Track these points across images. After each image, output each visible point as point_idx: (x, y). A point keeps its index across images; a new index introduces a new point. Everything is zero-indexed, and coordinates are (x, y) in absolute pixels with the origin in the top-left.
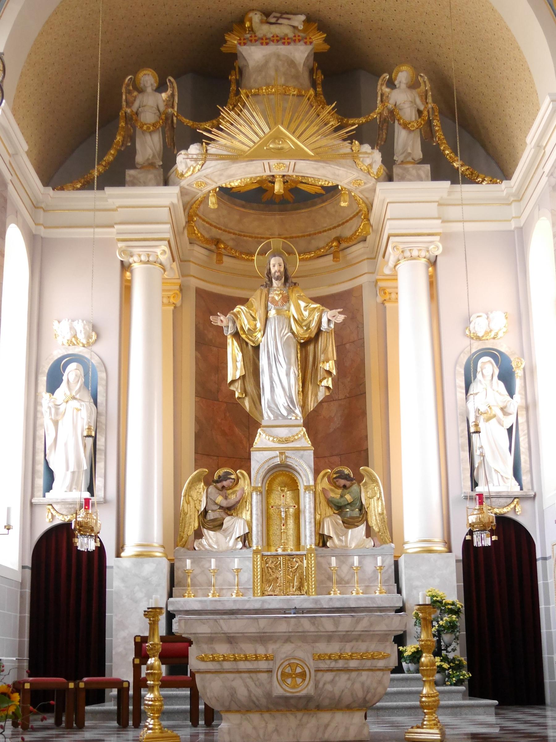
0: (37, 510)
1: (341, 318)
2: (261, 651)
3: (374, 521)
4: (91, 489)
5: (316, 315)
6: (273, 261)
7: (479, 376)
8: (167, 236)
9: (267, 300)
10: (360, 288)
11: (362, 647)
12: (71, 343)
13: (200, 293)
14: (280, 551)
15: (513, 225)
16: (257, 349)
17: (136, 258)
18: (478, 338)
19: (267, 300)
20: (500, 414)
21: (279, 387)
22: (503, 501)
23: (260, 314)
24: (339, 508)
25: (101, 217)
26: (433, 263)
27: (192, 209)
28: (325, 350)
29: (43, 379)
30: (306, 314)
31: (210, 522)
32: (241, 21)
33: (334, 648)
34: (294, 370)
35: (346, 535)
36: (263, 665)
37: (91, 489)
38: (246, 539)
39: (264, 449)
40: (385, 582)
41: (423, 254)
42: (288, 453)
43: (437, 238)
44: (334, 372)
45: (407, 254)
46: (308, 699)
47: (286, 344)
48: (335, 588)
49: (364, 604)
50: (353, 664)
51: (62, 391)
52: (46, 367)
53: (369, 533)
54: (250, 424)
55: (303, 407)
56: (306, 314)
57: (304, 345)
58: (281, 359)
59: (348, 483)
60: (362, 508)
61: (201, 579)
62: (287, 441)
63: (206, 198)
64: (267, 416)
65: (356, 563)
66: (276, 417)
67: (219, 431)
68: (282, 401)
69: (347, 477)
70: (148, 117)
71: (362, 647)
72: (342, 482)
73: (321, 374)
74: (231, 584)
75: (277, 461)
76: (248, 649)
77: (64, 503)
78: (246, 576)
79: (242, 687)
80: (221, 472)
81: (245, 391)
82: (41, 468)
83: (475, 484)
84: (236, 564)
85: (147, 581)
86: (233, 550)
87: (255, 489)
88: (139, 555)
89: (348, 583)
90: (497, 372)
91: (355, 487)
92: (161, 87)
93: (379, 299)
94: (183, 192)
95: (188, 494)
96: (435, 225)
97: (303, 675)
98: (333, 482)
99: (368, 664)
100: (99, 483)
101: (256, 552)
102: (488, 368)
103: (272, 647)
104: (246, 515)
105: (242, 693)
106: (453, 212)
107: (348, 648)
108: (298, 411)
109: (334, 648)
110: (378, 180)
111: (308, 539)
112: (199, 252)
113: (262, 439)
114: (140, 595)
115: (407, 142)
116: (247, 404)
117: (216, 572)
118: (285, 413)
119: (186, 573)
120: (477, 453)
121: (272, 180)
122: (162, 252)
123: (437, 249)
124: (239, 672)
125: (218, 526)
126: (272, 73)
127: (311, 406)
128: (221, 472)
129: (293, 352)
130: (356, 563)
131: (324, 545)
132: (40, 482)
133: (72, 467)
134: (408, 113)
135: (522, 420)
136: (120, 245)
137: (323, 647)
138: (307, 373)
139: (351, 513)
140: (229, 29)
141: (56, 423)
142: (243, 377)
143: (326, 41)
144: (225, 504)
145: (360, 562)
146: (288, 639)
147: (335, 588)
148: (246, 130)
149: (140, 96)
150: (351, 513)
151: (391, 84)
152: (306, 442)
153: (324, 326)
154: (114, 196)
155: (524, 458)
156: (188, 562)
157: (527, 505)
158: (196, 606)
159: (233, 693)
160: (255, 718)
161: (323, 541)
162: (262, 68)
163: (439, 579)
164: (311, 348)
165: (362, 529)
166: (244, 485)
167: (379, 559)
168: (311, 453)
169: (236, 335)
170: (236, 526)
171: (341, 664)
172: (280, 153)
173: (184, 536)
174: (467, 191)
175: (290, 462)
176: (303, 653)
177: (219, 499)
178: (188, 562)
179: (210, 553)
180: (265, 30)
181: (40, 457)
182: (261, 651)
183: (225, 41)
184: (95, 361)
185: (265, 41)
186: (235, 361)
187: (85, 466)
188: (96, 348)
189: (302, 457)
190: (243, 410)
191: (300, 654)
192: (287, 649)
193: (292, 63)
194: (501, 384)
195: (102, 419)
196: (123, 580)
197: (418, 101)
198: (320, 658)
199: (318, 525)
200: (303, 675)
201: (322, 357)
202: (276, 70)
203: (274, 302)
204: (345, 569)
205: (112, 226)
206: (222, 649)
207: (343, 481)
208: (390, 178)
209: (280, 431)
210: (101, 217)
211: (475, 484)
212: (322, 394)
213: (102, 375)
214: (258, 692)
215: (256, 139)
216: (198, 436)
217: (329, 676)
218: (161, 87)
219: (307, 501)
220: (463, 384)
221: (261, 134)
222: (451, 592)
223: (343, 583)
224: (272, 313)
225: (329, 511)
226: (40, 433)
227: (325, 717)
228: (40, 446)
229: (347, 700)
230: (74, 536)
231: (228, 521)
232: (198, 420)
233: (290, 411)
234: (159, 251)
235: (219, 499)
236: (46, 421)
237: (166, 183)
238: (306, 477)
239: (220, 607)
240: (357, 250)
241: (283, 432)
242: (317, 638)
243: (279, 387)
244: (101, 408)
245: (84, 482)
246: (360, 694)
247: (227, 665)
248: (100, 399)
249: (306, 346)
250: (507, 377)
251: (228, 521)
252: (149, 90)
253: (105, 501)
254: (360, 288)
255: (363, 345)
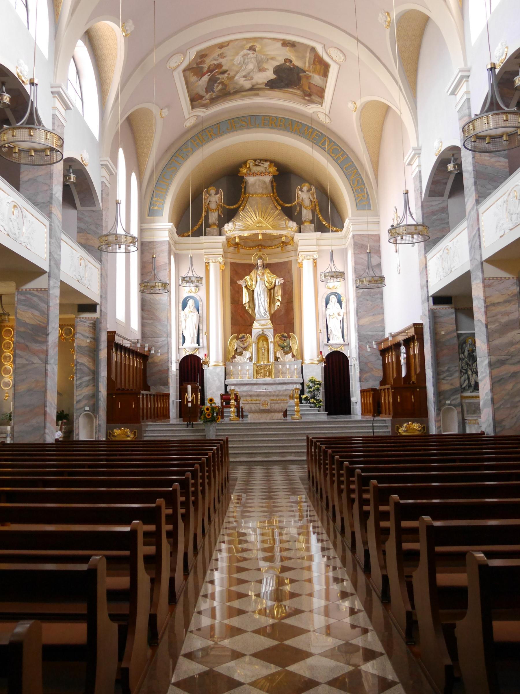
0: (180, 351)
1: (283, 281)
2: (258, 399)
3: (294, 352)
4: (198, 342)
5: (274, 279)
6: (259, 261)
7: (330, 302)
8: (222, 253)
9: (257, 273)
10: (291, 261)
11: (281, 398)
12: (190, 292)
13: (231, 264)
14: (262, 363)
15: (343, 247)
16: (253, 291)
17: (211, 261)
18: (330, 288)
19: (257, 273)
20: (337, 315)
21: (261, 308)
22: (338, 346)
23: (254, 279)
24: (283, 348)
25: (198, 246)
26: (315, 260)
27: (228, 240)
28: (277, 292)
29: (181, 305)
30: (270, 279)
31: (238, 353)
32: (245, 163)
33: (275, 398)
34: (267, 300)
35: (285, 357)
36: (258, 402)
37: (198, 342)
38: (250, 359)
39: (257, 327)
40: (298, 373)
41: (312, 258)
42: (265, 330)
43: (316, 253)
44: (280, 300)
45: (306, 258)
46: (269, 410)
47: (264, 290)
48: (281, 376)
49: (290, 381)
50: (279, 402)
51: (187, 309)
52: (181, 301)
53: (293, 356)
54: (252, 319)
55: (270, 312)
56: (270, 279)
57: (270, 290)
58: (262, 295)
59: (285, 339)
60: (290, 347)
61: (236, 372)
62: (264, 325)
63: (235, 238)
64: (257, 316)
65: (288, 367)
66: (261, 316)
67: (240, 320)
68: (262, 310)
69: (285, 337)
70: (213, 206)
71: (281, 398)
72: (284, 338)
73: (276, 301)
74: (246, 374)
75: (261, 333)
76: (255, 398)
77: (189, 348)
78: (251, 372)
79: (253, 407)
80: (241, 335)
81: (249, 307)
82: (181, 336)
83: (328, 339)
84: (247, 368)
85: (218, 374)
86: (246, 362)
87: (254, 342)
88: (215, 365)
89: (285, 373)
90: (337, 300)
91: (288, 340)
92: (217, 193)
93: (298, 266)
94: (226, 236)
95: (230, 343)
96: (315, 248)
97: (267, 404)
98: (280, 338)
99: (283, 402)
100: (201, 341)
101: (254, 364)
102: (333, 299)
103: (260, 398)
104: (250, 350)
105: (253, 409)
106: (322, 242)
107: (278, 398)
108: (268, 314)
109: (275, 398)
110: (296, 232)
111: (272, 359)
112: (231, 249)
113: (255, 325)
114: (216, 379)
115: (307, 214)
116: (250, 311)
117: (241, 371)
118: (263, 315)
119: (231, 371)
120: (329, 330)
121: (257, 234)
122: (220, 259)
123: (316, 257)
124: (278, 403)
125: (241, 354)
126: (257, 187)
127: (273, 312)
128: (241, 335)
129: (266, 293)
130: (288, 367)
131: (277, 360)
132: (181, 341)
133: (192, 336)
134: (307, 203)
135: (345, 318)
136: (206, 256)
137: (272, 398)
138: (271, 300)
139: (287, 349)
140: (241, 167)
141: (186, 320)
142: (249, 302)
143: (277, 170)
144: (243, 346)
145: (289, 367)
146: (264, 396)
147: (281, 376)
148: (249, 219)
149: (210, 197)
150: (287, 349)
151: (301, 190)
152: (271, 326)
153: (277, 284)
154: (202, 239)
155: (345, 331)
156: (231, 367)
157: (346, 347)
158: (235, 383)
159: (251, 408)
160: (257, 414)
161: (277, 359)
162: (254, 185)
163: (315, 372)
164: (272, 291)
165: (290, 355)
166: (249, 340)
167: (296, 366)
168: (272, 330)
169: (246, 287)
170: (247, 354)
171: (276, 402)
172: (260, 228)
173: (229, 357)
174: (326, 235)
175: (265, 333)
176: (268, 399)
177: (241, 345)
178: (231, 367)
179: (238, 364)
180: (255, 169)
181: (181, 332)
182: (258, 399)
183: (240, 171)
184: (198, 298)
185: (255, 174)
186: (246, 296)
187: (196, 335)
188: (199, 294)
189: (269, 331)
190: (249, 313)
191: (266, 399)
192: (264, 398)
193: (265, 183)
194: (338, 304)
195: (201, 319)
196: (210, 374)
197: (311, 197)
198: (271, 400)
199: (275, 353)
200: (267, 404)
201: (276, 295)
202: (259, 186)
203: (259, 275)
204: (284, 369)
205: (202, 249)
206: (249, 398)
207: (284, 338)
208: (300, 231)
209: (262, 323)
210: (198, 246)
211: (328, 339)
212: (276, 308)
213: (200, 303)
214: (257, 408)
215: (253, 223)
216: (232, 318)
217: (273, 405)
218: (217, 193)
219: (271, 346)
220: (325, 305)
221: (254, 221)
222: (319, 376)
223: (284, 374)
224: (259, 279)
225: (279, 348)
226: (180, 324)
227: (273, 414)
228: (180, 328)
229: (278, 410)
230: (202, 365)
231: (244, 352)
232: (232, 313)
233: (265, 314)
234: (219, 259)
235: (241, 345)
236: (182, 319)
237: (220, 235)
238: (271, 338)
239: (243, 383)
240: (289, 247)
241: (263, 322)
242: (270, 396)
243: (261, 308)
244: (201, 315)
245: (195, 341)
246: (281, 408)
247: (250, 402)
248: (200, 312)
249: (271, 290)
250: (340, 302)
251: (244, 352)
252: (213, 195)
253: (203, 347)
254: (291, 261)
255: (292, 284)
